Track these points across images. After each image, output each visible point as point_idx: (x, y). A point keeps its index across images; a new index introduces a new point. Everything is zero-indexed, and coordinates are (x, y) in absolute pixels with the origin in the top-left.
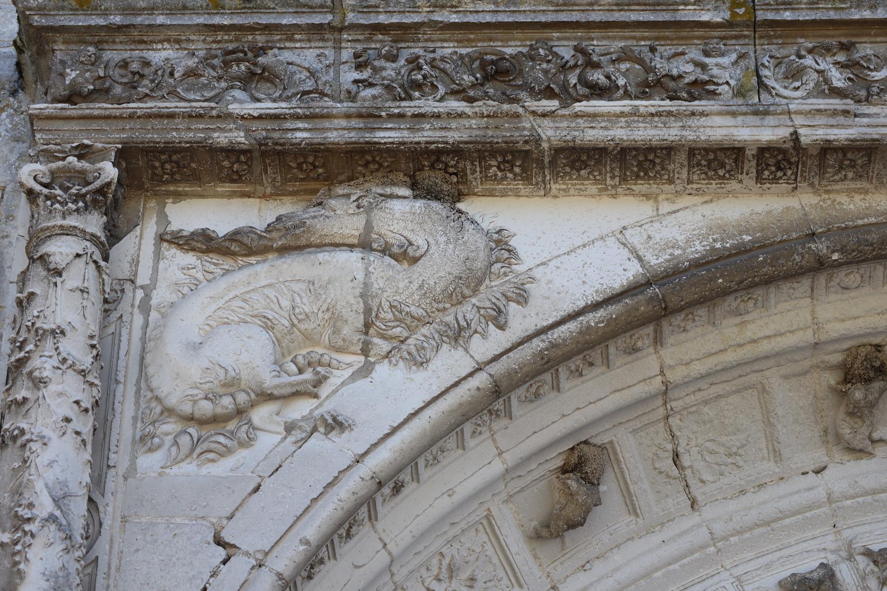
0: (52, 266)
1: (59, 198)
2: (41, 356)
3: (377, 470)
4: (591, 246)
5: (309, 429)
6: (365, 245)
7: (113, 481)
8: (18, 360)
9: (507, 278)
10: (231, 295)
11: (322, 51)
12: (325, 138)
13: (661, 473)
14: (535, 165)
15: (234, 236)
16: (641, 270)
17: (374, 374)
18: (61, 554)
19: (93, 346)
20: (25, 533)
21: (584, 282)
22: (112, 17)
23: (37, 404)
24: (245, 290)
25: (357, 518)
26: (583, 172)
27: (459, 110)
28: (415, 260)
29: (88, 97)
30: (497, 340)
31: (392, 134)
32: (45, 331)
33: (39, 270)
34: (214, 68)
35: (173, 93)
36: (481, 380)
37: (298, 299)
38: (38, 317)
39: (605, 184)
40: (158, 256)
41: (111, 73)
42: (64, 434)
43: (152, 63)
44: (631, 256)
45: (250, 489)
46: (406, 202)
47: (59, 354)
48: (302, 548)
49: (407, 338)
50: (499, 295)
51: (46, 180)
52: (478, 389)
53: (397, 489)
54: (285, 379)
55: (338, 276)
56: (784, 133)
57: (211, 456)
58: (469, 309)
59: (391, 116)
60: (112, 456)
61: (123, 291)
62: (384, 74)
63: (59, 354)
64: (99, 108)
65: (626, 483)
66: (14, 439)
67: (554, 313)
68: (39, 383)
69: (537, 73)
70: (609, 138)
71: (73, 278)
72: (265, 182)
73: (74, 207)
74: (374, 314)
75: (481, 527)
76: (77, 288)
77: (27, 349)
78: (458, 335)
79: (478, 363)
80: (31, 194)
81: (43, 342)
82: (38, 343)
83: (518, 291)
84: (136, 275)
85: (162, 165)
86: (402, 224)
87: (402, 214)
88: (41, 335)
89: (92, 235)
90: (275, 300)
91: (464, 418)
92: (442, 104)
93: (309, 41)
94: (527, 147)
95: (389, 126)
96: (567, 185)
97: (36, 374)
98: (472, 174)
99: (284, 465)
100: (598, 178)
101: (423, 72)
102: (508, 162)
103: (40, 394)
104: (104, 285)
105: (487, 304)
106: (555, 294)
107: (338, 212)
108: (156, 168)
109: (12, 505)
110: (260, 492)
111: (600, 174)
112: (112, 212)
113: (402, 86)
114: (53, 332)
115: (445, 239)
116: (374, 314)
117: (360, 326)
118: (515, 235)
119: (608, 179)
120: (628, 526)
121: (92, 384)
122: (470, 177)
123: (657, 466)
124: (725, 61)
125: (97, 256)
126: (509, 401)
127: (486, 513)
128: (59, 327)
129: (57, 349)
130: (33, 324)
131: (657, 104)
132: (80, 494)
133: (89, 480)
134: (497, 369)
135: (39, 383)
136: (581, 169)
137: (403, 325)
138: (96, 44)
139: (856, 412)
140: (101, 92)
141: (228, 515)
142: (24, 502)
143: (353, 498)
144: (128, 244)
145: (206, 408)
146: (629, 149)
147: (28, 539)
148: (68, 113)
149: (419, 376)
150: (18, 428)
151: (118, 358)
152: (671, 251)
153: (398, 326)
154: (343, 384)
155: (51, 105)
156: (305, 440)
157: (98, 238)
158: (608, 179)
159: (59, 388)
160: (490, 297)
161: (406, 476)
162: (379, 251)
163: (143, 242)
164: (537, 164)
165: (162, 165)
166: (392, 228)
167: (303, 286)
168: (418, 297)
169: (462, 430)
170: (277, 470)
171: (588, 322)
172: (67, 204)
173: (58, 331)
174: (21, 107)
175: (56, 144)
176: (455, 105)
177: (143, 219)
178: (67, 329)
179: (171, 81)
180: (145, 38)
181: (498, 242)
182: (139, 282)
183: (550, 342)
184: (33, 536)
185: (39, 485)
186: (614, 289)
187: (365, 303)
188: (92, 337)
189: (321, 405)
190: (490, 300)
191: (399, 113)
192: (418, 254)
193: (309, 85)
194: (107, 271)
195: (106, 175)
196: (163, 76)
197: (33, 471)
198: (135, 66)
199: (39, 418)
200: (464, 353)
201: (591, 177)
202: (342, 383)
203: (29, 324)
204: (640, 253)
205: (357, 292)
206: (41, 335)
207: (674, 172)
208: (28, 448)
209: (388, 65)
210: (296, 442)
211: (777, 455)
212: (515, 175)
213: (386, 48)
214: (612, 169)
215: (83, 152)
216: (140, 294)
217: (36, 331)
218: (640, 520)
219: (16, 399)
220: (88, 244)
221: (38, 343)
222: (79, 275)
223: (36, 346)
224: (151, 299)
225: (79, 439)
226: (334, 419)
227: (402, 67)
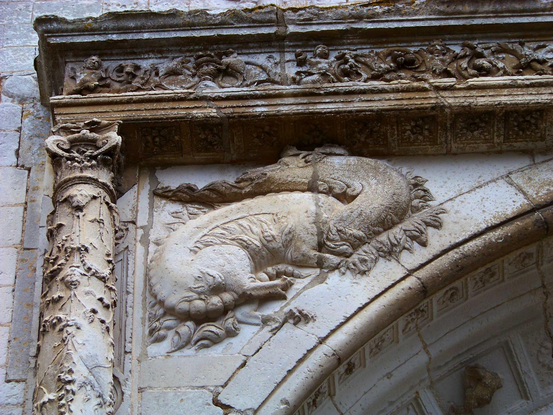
0: (75, 204)
1: (76, 159)
2: (70, 267)
3: (336, 348)
4: (486, 186)
5: (281, 321)
7: (130, 363)
8: (51, 272)
9: (425, 210)
10: (213, 226)
11: (270, 54)
12: (278, 111)
13: (544, 366)
14: (439, 127)
16: (526, 201)
17: (327, 281)
18: (96, 407)
19: (109, 262)
20: (68, 391)
21: (484, 211)
22: (109, 35)
23: (70, 300)
24: (224, 222)
25: (321, 390)
26: (476, 133)
27: (380, 87)
28: (354, 197)
31: (331, 106)
32: (72, 248)
33: (65, 209)
34: (188, 69)
35: (159, 86)
36: (411, 282)
37: (265, 226)
38: (66, 240)
39: (493, 143)
40: (152, 206)
41: (110, 75)
42: (92, 321)
43: (141, 67)
44: (517, 192)
45: (238, 365)
46: (342, 158)
47: (84, 265)
48: (282, 407)
49: (351, 254)
50: (420, 222)
51: (66, 147)
52: (410, 288)
53: (350, 370)
54: (259, 283)
55: (290, 210)
57: (205, 342)
58: (398, 231)
59: (328, 94)
60: (128, 345)
61: (127, 229)
62: (320, 66)
63: (84, 265)
64: (103, 97)
65: (519, 374)
66: (54, 326)
67: (463, 233)
68: (70, 285)
70: (496, 103)
72: (232, 149)
73: (89, 164)
74: (325, 236)
75: (410, 407)
76: (95, 219)
77: (60, 263)
78: (391, 252)
79: (408, 270)
80: (54, 156)
81: (72, 258)
82: (68, 258)
83: (434, 218)
84: (136, 218)
85: (154, 138)
86: (341, 173)
87: (338, 166)
88: (70, 252)
89: (104, 184)
90: (248, 227)
92: (366, 84)
93: (260, 47)
94: (434, 113)
95: (327, 101)
96: (464, 144)
97: (68, 278)
98: (392, 137)
99: (263, 347)
100: (487, 137)
101: (350, 63)
102: (418, 126)
103: (72, 293)
104: (114, 220)
105: (412, 228)
106: (463, 220)
107: (291, 166)
108: (148, 142)
109: (56, 372)
110: (246, 368)
111: (489, 133)
113: (334, 74)
114: (79, 249)
115: (375, 181)
116: (325, 236)
117: (315, 245)
118: (427, 181)
119: (495, 138)
120: (521, 407)
121: (111, 289)
122: (390, 139)
123: (541, 360)
125: (108, 199)
126: (432, 303)
127: (414, 395)
128: (83, 246)
129: (82, 262)
130: (63, 245)
132: (107, 366)
133: (113, 358)
134: (422, 273)
136: (475, 130)
137: (348, 244)
138: (100, 56)
141: (223, 384)
142: (64, 370)
143: (320, 369)
144: (129, 196)
145: (199, 304)
146: (512, 112)
147: (70, 396)
148: (80, 100)
149: (364, 281)
150: (57, 318)
151: (127, 276)
152: (547, 187)
153: (344, 244)
154: (305, 288)
155: (67, 96)
156: (278, 329)
157: (108, 187)
158: (495, 138)
159: (87, 289)
160: (413, 223)
161: (355, 358)
162: (324, 193)
163: (140, 196)
164: (441, 127)
165: (154, 138)
166: (333, 176)
167: (269, 217)
168: (358, 223)
169: (397, 324)
170: (258, 351)
171: (489, 238)
172: (83, 162)
173: (83, 249)
174: (39, 114)
175: (72, 123)
177: (139, 181)
178: (90, 248)
179: (157, 79)
180: (135, 50)
181: (416, 185)
182: (139, 224)
183: (462, 254)
184: (74, 393)
185: (75, 358)
186: (508, 215)
187: (318, 228)
188: (108, 255)
189: (288, 304)
190: (413, 225)
191: (334, 91)
192: (355, 193)
193: (264, 77)
194: (117, 210)
195: (113, 140)
196: (150, 75)
197: (70, 347)
198: (128, 69)
199: (72, 310)
200: (396, 263)
201: (482, 137)
202: (304, 288)
203: (60, 245)
204: (525, 190)
205: (312, 219)
206: (70, 252)
207: (545, 131)
208: (65, 331)
209: (322, 60)
210: (271, 331)
211: (525, 394)
212: (424, 137)
213: (320, 49)
214: (499, 129)
215: (94, 127)
216: (140, 232)
217: (66, 250)
218: (530, 402)
219: (53, 298)
220: (101, 190)
221: (68, 258)
223: (67, 260)
224: (149, 235)
225: (104, 326)
226: (300, 312)
227: (333, 62)
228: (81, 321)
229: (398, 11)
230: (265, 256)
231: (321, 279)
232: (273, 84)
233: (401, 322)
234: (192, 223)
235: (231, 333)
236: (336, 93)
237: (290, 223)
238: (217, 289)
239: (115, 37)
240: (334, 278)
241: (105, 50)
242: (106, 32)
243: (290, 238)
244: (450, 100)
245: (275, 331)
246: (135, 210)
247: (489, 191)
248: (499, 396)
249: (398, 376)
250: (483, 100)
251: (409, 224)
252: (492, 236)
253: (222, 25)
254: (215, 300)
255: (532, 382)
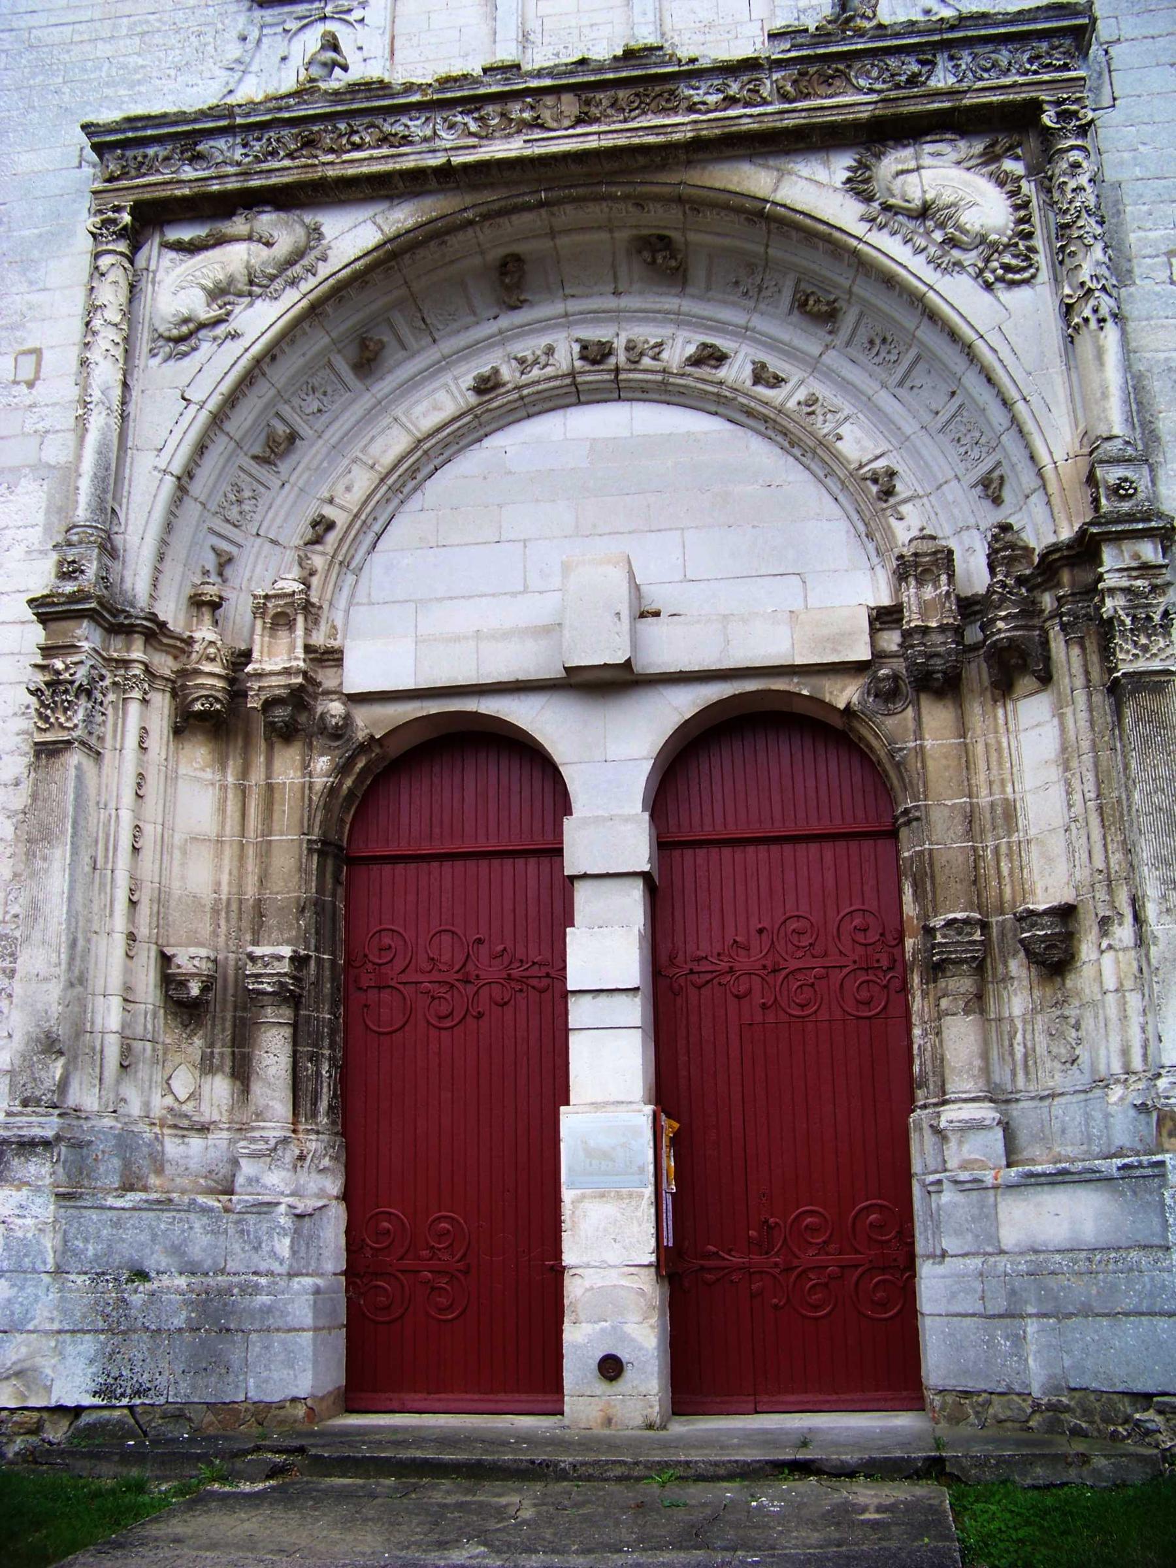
6: (250, 238)
15: (191, 242)
29: (118, 179)
30: (312, 282)
35: (158, 171)
36: (304, 303)
53: (274, 358)
55: (234, 258)
56: (444, 160)
59: (256, 173)
68: (95, 333)
69: (327, 141)
71: (111, 277)
78: (293, 283)
87: (267, 221)
91: (367, 278)
112: (135, 237)
124: (418, 123)
131: (385, 151)
134: (311, 296)
135: (95, 333)
139: (508, 289)
140: (124, 175)
144: (145, 250)
145: (175, 332)
161: (276, 351)
176: (287, 163)
211: (404, 348)
215: (117, 209)
222: (117, 275)
228: (99, 359)
229: (305, 102)
230: (219, 293)
231: (251, 305)
232: (227, 163)
233: (306, 325)
234: (184, 266)
235: (194, 349)
236: (261, 172)
237: (231, 269)
238: (186, 321)
239: (130, 135)
240: (259, 303)
241: (125, 144)
242: (124, 131)
243: (231, 280)
244: (331, 172)
245: (220, 345)
246: (149, 259)
247: (360, 230)
248: (387, 352)
249: (308, 357)
250: (351, 171)
251: (305, 262)
252: (357, 265)
253: (195, 121)
254: (185, 329)
255: (409, 339)
